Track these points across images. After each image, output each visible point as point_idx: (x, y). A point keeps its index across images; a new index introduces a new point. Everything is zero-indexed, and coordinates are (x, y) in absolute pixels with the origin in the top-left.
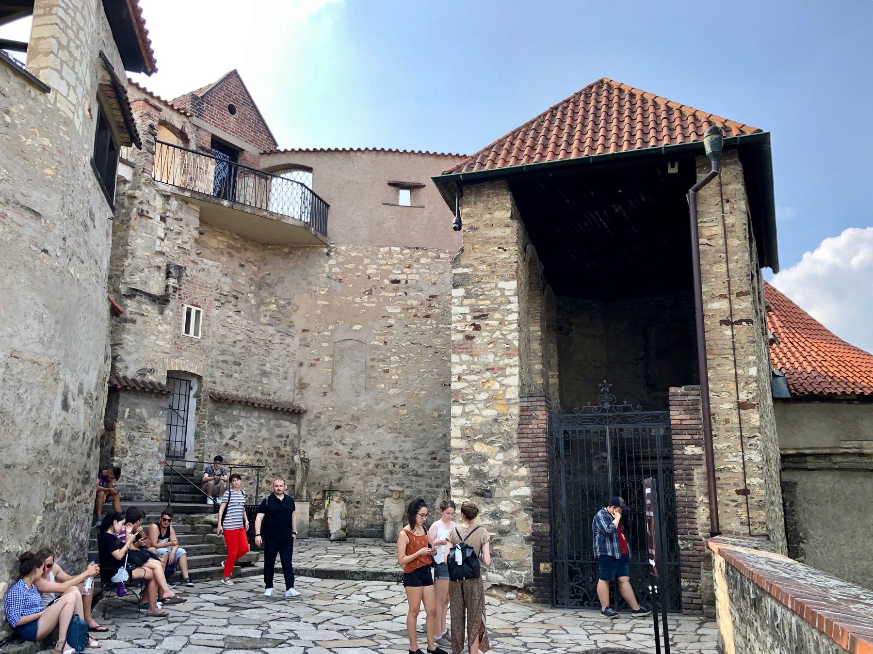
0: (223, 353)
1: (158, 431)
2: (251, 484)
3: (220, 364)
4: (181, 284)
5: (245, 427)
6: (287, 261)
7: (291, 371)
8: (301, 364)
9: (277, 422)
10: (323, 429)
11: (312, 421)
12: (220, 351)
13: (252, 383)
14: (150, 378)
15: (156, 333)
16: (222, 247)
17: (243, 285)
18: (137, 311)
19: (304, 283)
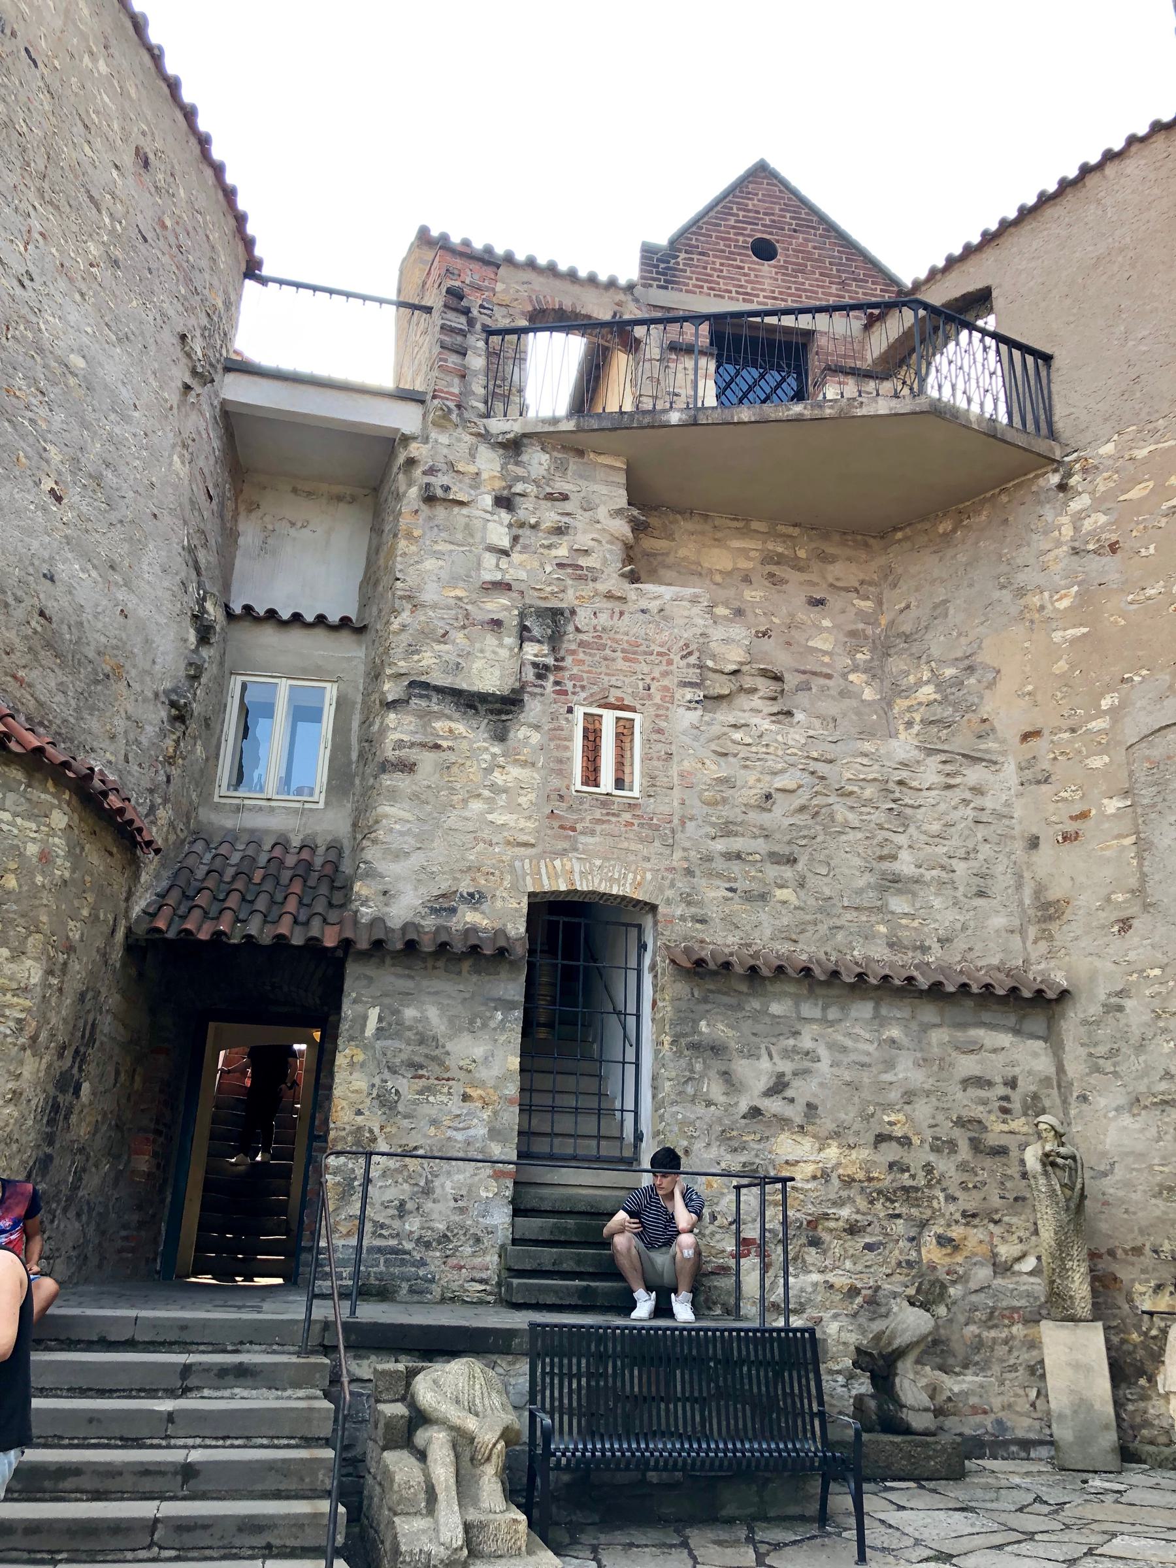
0: (727, 830)
1: (487, 1074)
2: (869, 1247)
3: (719, 864)
4: (562, 653)
5: (822, 1052)
6: (950, 552)
7: (1000, 868)
8: (1034, 843)
9: (960, 1035)
10: (1140, 1048)
11: (1097, 1023)
12: (713, 825)
13: (850, 915)
14: (470, 917)
15: (486, 793)
16: (744, 564)
17: (825, 653)
18: (418, 738)
19: (1006, 595)
